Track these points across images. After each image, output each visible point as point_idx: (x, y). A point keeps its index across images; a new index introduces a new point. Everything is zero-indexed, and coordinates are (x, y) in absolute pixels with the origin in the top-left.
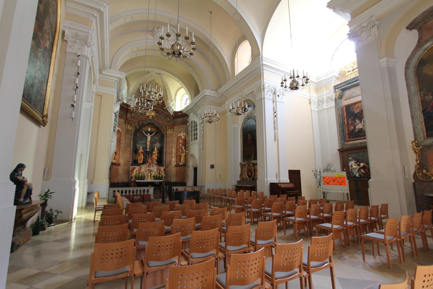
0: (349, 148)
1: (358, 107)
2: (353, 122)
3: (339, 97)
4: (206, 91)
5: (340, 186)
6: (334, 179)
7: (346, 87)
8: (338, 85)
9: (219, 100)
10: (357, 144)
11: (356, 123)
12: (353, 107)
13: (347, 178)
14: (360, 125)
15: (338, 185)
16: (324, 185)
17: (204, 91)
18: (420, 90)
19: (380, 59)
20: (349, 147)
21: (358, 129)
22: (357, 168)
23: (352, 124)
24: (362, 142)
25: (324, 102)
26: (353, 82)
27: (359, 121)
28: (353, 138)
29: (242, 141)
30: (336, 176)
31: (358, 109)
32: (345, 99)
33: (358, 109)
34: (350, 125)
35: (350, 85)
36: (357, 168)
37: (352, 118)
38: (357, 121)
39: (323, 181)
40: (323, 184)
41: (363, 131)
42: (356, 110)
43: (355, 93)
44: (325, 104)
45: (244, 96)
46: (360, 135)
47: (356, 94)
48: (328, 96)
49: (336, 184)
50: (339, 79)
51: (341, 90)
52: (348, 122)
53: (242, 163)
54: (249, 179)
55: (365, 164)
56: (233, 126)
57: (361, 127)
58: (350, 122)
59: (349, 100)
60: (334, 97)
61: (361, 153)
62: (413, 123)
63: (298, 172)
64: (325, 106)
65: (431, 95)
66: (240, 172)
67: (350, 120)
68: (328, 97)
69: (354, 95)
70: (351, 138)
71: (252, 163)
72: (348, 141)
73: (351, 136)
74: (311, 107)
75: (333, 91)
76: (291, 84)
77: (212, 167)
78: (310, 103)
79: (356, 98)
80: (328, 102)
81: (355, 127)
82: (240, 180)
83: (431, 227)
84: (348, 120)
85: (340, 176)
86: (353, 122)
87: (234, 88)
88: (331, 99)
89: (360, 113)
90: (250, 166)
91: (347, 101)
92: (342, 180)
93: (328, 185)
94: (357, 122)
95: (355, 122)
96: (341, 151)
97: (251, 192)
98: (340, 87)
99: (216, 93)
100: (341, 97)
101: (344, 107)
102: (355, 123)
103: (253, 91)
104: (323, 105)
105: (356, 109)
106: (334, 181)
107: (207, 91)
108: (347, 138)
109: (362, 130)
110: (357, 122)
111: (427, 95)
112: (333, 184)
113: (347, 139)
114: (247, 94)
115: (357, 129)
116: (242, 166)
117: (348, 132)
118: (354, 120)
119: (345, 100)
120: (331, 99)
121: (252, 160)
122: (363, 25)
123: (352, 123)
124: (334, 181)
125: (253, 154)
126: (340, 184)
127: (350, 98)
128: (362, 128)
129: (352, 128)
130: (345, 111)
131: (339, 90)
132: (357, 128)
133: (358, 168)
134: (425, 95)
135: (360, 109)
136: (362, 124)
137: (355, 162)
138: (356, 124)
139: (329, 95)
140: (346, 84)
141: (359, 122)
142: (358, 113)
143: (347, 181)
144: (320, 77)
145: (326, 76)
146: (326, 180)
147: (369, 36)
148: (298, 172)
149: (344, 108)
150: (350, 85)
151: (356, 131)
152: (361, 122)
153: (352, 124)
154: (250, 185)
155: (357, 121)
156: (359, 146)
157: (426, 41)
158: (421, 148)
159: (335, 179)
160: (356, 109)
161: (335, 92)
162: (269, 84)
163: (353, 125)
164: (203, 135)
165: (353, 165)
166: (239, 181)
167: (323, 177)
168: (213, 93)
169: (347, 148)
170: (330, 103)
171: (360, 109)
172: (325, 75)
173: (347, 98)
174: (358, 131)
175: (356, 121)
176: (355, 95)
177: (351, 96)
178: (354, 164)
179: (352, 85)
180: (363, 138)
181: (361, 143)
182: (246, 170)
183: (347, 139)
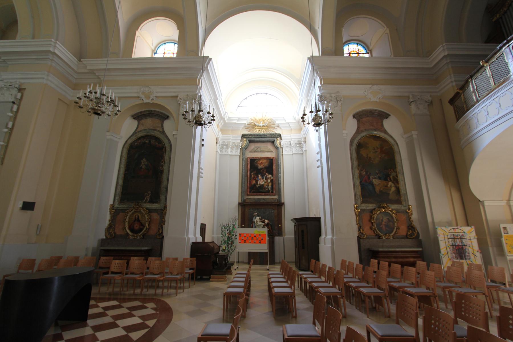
0: (252, 203)
1: (261, 162)
2: (255, 176)
3: (246, 147)
4: (57, 45)
5: (259, 244)
6: (253, 236)
7: (254, 140)
8: (247, 135)
9: (76, 77)
10: (260, 199)
11: (258, 178)
12: (258, 162)
13: (268, 235)
14: (262, 181)
15: (257, 243)
16: (240, 244)
17: (52, 43)
18: (359, 165)
19: (343, 130)
20: (252, 202)
21: (260, 184)
22: (262, 224)
23: (255, 178)
24: (265, 198)
25: (229, 147)
26: (262, 137)
27: (261, 177)
28: (253, 192)
29: (123, 166)
30: (256, 233)
31: (262, 165)
32: (249, 151)
33: (262, 165)
34: (252, 179)
35: (258, 139)
36: (262, 224)
37: (255, 172)
38: (260, 177)
39: (239, 239)
40: (238, 242)
41: (264, 187)
42: (260, 165)
43: (260, 148)
44: (229, 149)
45: (151, 96)
46: (261, 191)
47: (261, 150)
48: (234, 141)
49: (254, 243)
50: (247, 129)
51: (249, 140)
52: (250, 175)
53: (116, 205)
54: (132, 236)
55: (269, 221)
56: (109, 137)
57: (263, 183)
58: (253, 176)
59: (254, 153)
60: (241, 145)
61: (263, 209)
62: (354, 190)
63: (205, 225)
64: (229, 151)
65: (365, 171)
66: (107, 223)
67: (253, 173)
68: (234, 143)
69: (259, 150)
70: (252, 192)
71: (147, 209)
72: (248, 195)
73: (252, 191)
74: (217, 147)
75: (240, 138)
76: (314, 120)
77: (28, 206)
78: (216, 143)
79: (260, 153)
80: (232, 148)
81: (257, 181)
82: (104, 238)
83: (33, 272)
84: (252, 173)
85: (260, 233)
86: (255, 176)
87: (131, 74)
88: (237, 146)
89: (263, 169)
90: (141, 213)
91: (252, 153)
92: (262, 238)
93: (245, 244)
94: (260, 178)
95: (257, 177)
96: (243, 205)
97: (292, 262)
98: (249, 138)
99: (76, 63)
100: (246, 148)
101: (249, 158)
102: (257, 178)
103: (177, 97)
104: (227, 149)
105: (260, 164)
106: (252, 238)
107: (59, 45)
108: (248, 191)
109: (263, 186)
110: (260, 178)
111: (363, 170)
112: (250, 243)
113: (248, 193)
114: (159, 95)
115: (259, 185)
116: (115, 212)
117: (250, 186)
118: (257, 174)
119: (250, 152)
120: (237, 146)
121: (145, 203)
122: (333, 95)
123: (254, 177)
124: (252, 238)
125: (150, 192)
126: (260, 242)
127: (254, 152)
128: (263, 185)
129: (254, 182)
130: (249, 163)
131: (247, 140)
132: (258, 184)
133: (263, 225)
134: (361, 171)
135: (263, 166)
136: (264, 180)
137: (260, 218)
138: (258, 180)
139: (236, 142)
140: (255, 136)
141: (261, 178)
142: (261, 169)
143: (267, 238)
144: (232, 118)
145: (238, 120)
146: (243, 238)
147: (336, 107)
148: (205, 225)
149: (249, 160)
150: (258, 139)
151: (258, 186)
152: (263, 178)
153: (255, 178)
154: (146, 247)
155: (260, 177)
156: (261, 201)
157: (362, 131)
158: (359, 211)
159: (254, 236)
160: (260, 164)
161: (241, 140)
162: (205, 99)
163: (255, 179)
164: (12, 129)
165: (258, 221)
166: (104, 239)
167: (240, 234)
168: (72, 59)
169: (250, 203)
170: (234, 150)
171: (263, 166)
172: (238, 118)
173: (252, 151)
174: (259, 187)
175: (259, 177)
176: (260, 151)
177: (256, 150)
178: (259, 220)
179: (260, 140)
180: (263, 194)
181: (264, 199)
182: (127, 220)
183: (248, 193)
